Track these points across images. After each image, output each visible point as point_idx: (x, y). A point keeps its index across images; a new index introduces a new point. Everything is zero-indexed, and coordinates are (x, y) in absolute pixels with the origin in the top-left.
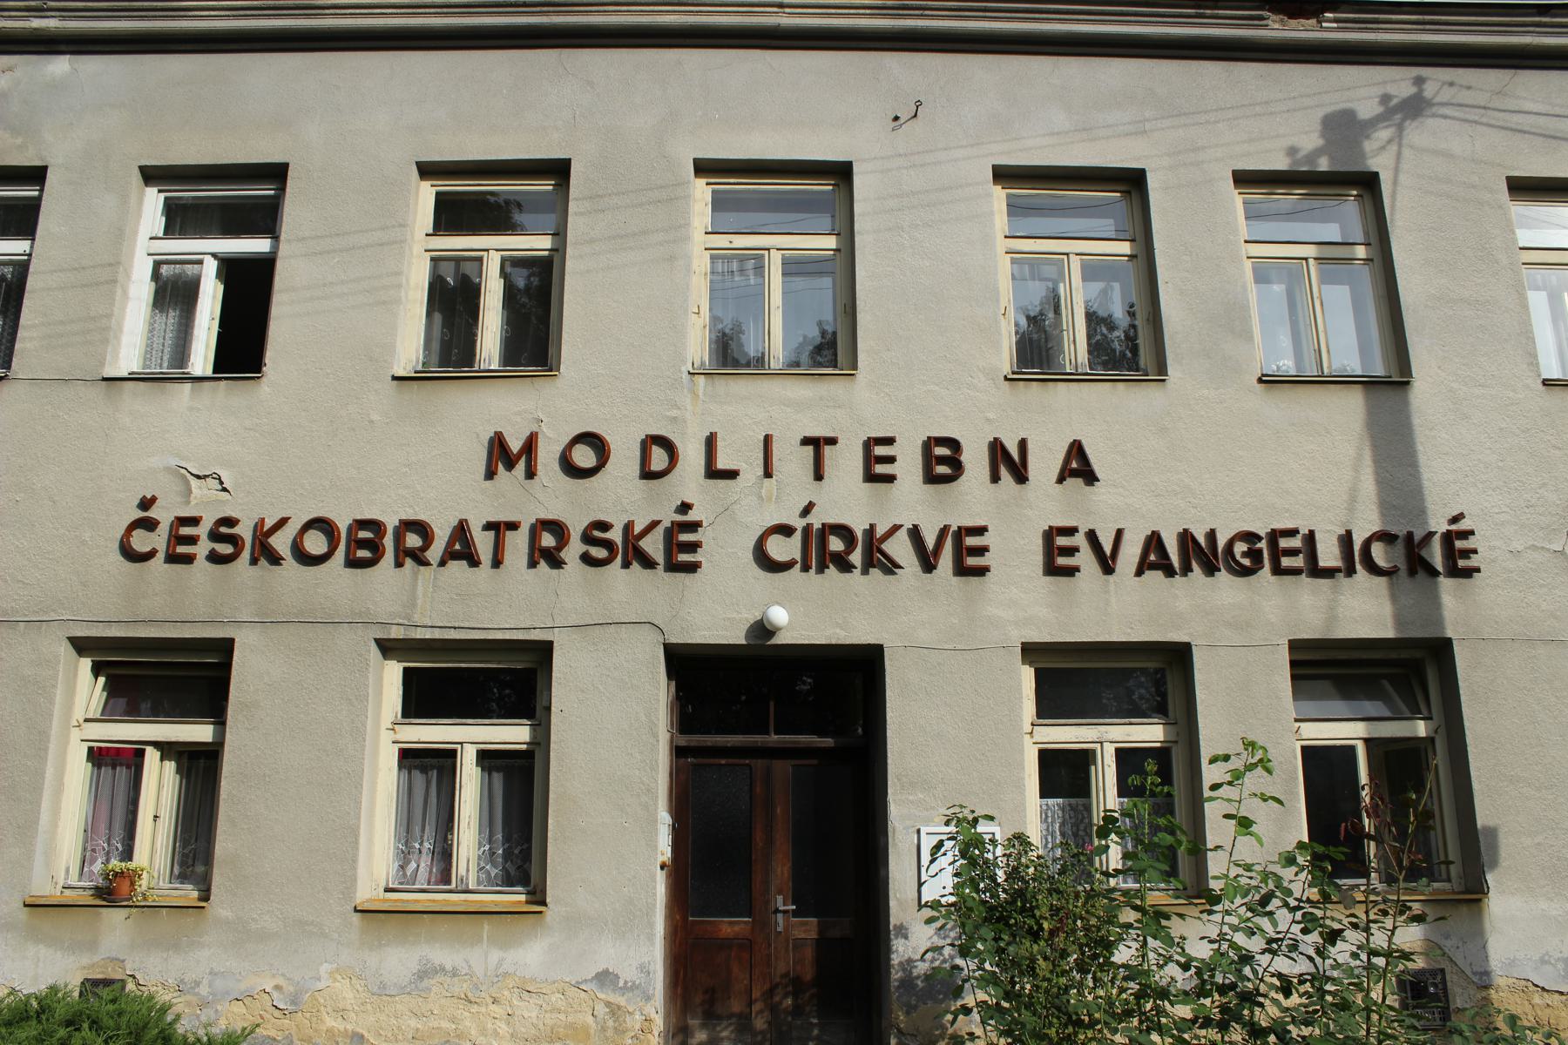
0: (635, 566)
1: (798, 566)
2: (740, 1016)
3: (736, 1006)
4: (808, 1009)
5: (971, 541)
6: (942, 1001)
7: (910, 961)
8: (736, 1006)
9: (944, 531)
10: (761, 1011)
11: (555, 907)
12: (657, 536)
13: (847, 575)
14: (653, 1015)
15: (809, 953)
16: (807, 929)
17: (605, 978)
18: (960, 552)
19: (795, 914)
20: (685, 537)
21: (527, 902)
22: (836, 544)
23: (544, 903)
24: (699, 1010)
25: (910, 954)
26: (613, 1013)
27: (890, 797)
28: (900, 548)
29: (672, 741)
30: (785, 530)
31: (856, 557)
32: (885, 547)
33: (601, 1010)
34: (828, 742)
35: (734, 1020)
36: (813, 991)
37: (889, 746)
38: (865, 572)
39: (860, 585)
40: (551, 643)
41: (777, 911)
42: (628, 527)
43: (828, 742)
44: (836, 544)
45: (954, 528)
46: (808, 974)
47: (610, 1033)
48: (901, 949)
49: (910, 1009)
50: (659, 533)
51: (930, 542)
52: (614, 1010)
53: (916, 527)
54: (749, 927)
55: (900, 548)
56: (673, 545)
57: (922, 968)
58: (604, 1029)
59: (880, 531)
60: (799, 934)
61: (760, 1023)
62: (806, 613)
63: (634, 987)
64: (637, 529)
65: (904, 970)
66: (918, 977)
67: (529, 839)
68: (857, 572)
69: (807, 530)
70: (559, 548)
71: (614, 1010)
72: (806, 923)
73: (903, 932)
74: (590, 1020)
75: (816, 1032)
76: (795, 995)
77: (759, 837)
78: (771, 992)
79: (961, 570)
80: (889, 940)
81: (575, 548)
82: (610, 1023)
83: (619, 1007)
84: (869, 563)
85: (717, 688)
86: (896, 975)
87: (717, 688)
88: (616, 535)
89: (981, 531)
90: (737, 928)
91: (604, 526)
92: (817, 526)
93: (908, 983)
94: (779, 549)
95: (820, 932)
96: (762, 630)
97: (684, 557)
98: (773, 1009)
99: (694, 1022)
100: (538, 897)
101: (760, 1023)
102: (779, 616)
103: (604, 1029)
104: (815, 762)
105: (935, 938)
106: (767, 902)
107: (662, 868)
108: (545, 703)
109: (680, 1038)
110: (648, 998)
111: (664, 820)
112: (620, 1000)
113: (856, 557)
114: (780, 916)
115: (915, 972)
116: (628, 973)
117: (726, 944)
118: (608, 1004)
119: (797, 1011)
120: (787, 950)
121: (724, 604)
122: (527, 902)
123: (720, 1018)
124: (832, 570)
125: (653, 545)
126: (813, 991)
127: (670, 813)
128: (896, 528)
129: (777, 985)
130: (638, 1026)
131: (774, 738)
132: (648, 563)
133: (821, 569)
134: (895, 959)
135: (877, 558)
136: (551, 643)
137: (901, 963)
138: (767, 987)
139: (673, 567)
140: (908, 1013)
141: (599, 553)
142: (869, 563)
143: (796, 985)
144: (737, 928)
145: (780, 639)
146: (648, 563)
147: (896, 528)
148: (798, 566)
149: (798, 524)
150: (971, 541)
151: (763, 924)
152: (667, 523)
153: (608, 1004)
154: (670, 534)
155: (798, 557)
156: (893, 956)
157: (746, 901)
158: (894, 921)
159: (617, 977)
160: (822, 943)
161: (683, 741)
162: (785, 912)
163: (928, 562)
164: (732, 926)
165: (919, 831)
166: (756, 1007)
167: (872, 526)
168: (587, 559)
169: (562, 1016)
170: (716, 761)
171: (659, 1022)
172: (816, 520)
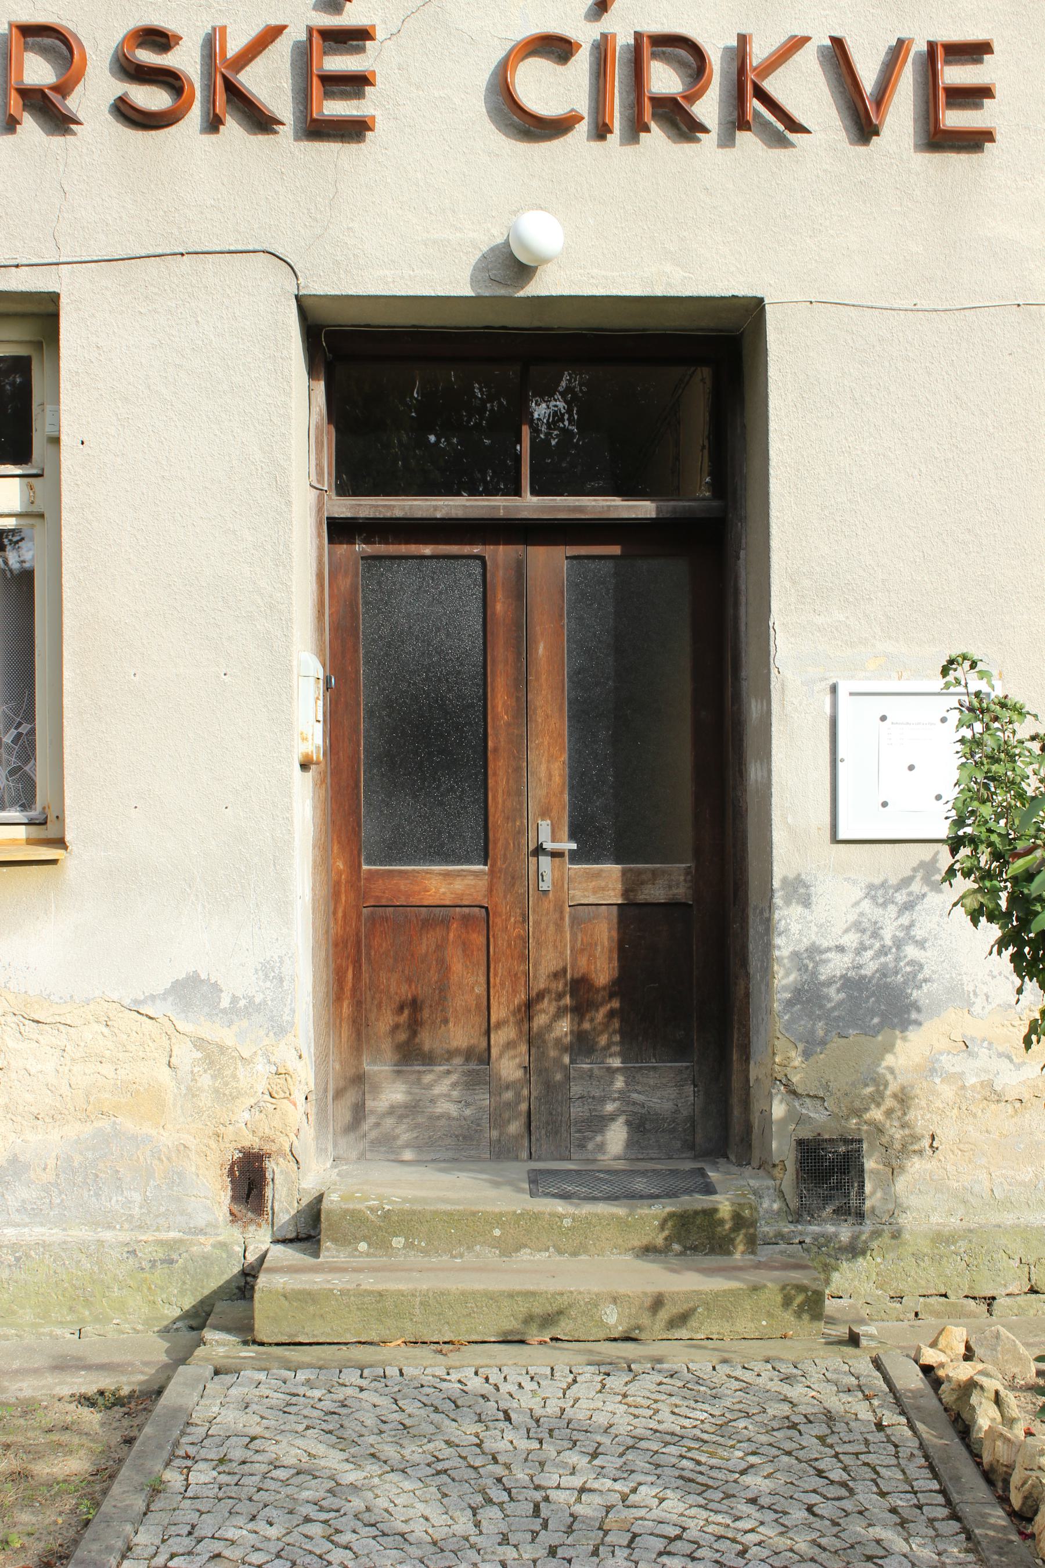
0: (232, 127)
1: (583, 128)
2: (469, 1054)
3: (460, 1035)
4: (603, 1040)
5: (954, 75)
6: (876, 1031)
7: (814, 950)
8: (460, 1035)
9: (897, 51)
10: (510, 1045)
11: (76, 860)
12: (278, 59)
13: (688, 147)
14: (292, 1063)
15: (604, 933)
16: (603, 884)
17: (191, 991)
18: (934, 96)
19: (575, 857)
20: (338, 63)
21: (30, 842)
22: (664, 79)
23: (60, 843)
24: (387, 1046)
25: (812, 936)
26: (210, 1061)
27: (776, 618)
28: (803, 88)
29: (320, 510)
30: (556, 47)
31: (708, 108)
32: (769, 85)
33: (186, 1055)
34: (645, 509)
35: (458, 1061)
36: (615, 1004)
37: (774, 513)
38: (727, 141)
39: (717, 167)
40: (54, 298)
41: (539, 850)
42: (211, 45)
43: (645, 509)
44: (664, 79)
45: (920, 46)
46: (603, 971)
47: (205, 1100)
48: (795, 928)
49: (811, 1046)
50: (278, 59)
51: (868, 77)
52: (212, 1055)
53: (838, 43)
54: (483, 883)
55: (803, 88)
56: (317, 83)
57: (836, 965)
58: (192, 1093)
59: (759, 53)
60: (582, 894)
61: (509, 1067)
62: (614, 232)
63: (252, 1008)
64: (234, 46)
65: (802, 968)
66: (830, 982)
67: (30, 716)
68: (709, 140)
69: (602, 50)
70: (63, 89)
71: (212, 1055)
72: (598, 875)
73: (800, 891)
74: (164, 1075)
75: (619, 1083)
76: (579, 1010)
77: (501, 702)
78: (529, 1008)
79: (937, 139)
80: (770, 907)
81: (95, 93)
82: (206, 1081)
83: (222, 1049)
84: (738, 121)
85: (418, 399)
86: (784, 979)
87: (418, 399)
88: (185, 59)
89: (974, 51)
90: (459, 885)
91: (158, 38)
92: (624, 39)
93: (808, 996)
94: (543, 88)
95: (625, 893)
96: (513, 265)
97: (336, 108)
98: (533, 1040)
99: (378, 1066)
100: (50, 832)
101: (509, 1067)
102: (542, 233)
103: (192, 1093)
104: (616, 550)
105: (866, 905)
106: (521, 832)
107: (304, 766)
108: (49, 430)
109: (351, 1097)
110: (281, 1030)
111: (306, 671)
112: (227, 1036)
113: (708, 108)
114: (545, 861)
115: (825, 973)
116: (238, 981)
117: (436, 917)
118: (199, 1043)
119: (582, 1044)
120: (559, 927)
121: (427, 217)
122: (30, 842)
123: (428, 1059)
124: (656, 136)
125: (270, 82)
126: (615, 1004)
127: (320, 653)
128: (797, 43)
129: (541, 996)
130: (261, 1086)
131: (529, 504)
132: (260, 121)
133: (636, 128)
134: (783, 947)
135: (753, 106)
136: (54, 298)
137: (795, 954)
138: (521, 997)
139: (318, 130)
140: (807, 1054)
141: (152, 98)
142: (738, 121)
143: (580, 994)
144: (459, 885)
145: (547, 284)
146: (260, 121)
147: (797, 43)
148: (583, 128)
149: (584, 34)
150: (954, 75)
151: (513, 880)
152: (296, 33)
153: (199, 1043)
154: (304, 56)
155: (582, 105)
156: (778, 941)
157: (472, 835)
158: (781, 870)
159: (216, 988)
160: (633, 915)
161: (345, 507)
162: (555, 855)
163: (864, 126)
164: (447, 882)
165: (834, 689)
166: (499, 1038)
167: (743, 40)
168: (127, 114)
169: (107, 1069)
170: (414, 549)
171: (305, 1075)
172: (622, 26)
